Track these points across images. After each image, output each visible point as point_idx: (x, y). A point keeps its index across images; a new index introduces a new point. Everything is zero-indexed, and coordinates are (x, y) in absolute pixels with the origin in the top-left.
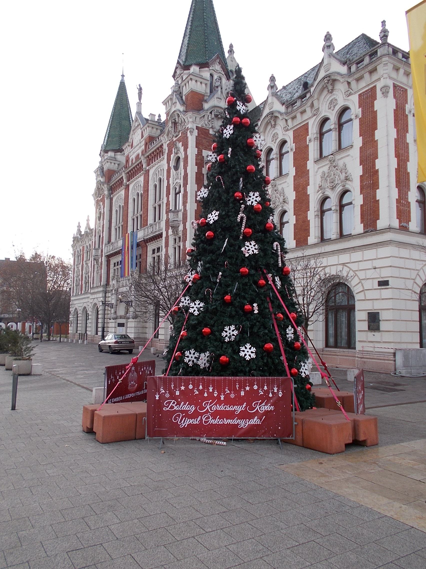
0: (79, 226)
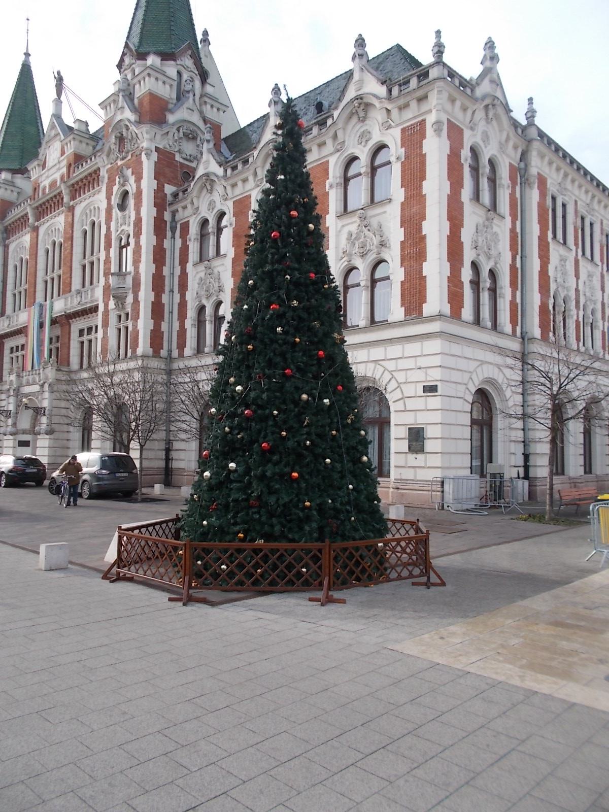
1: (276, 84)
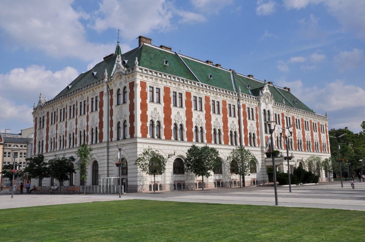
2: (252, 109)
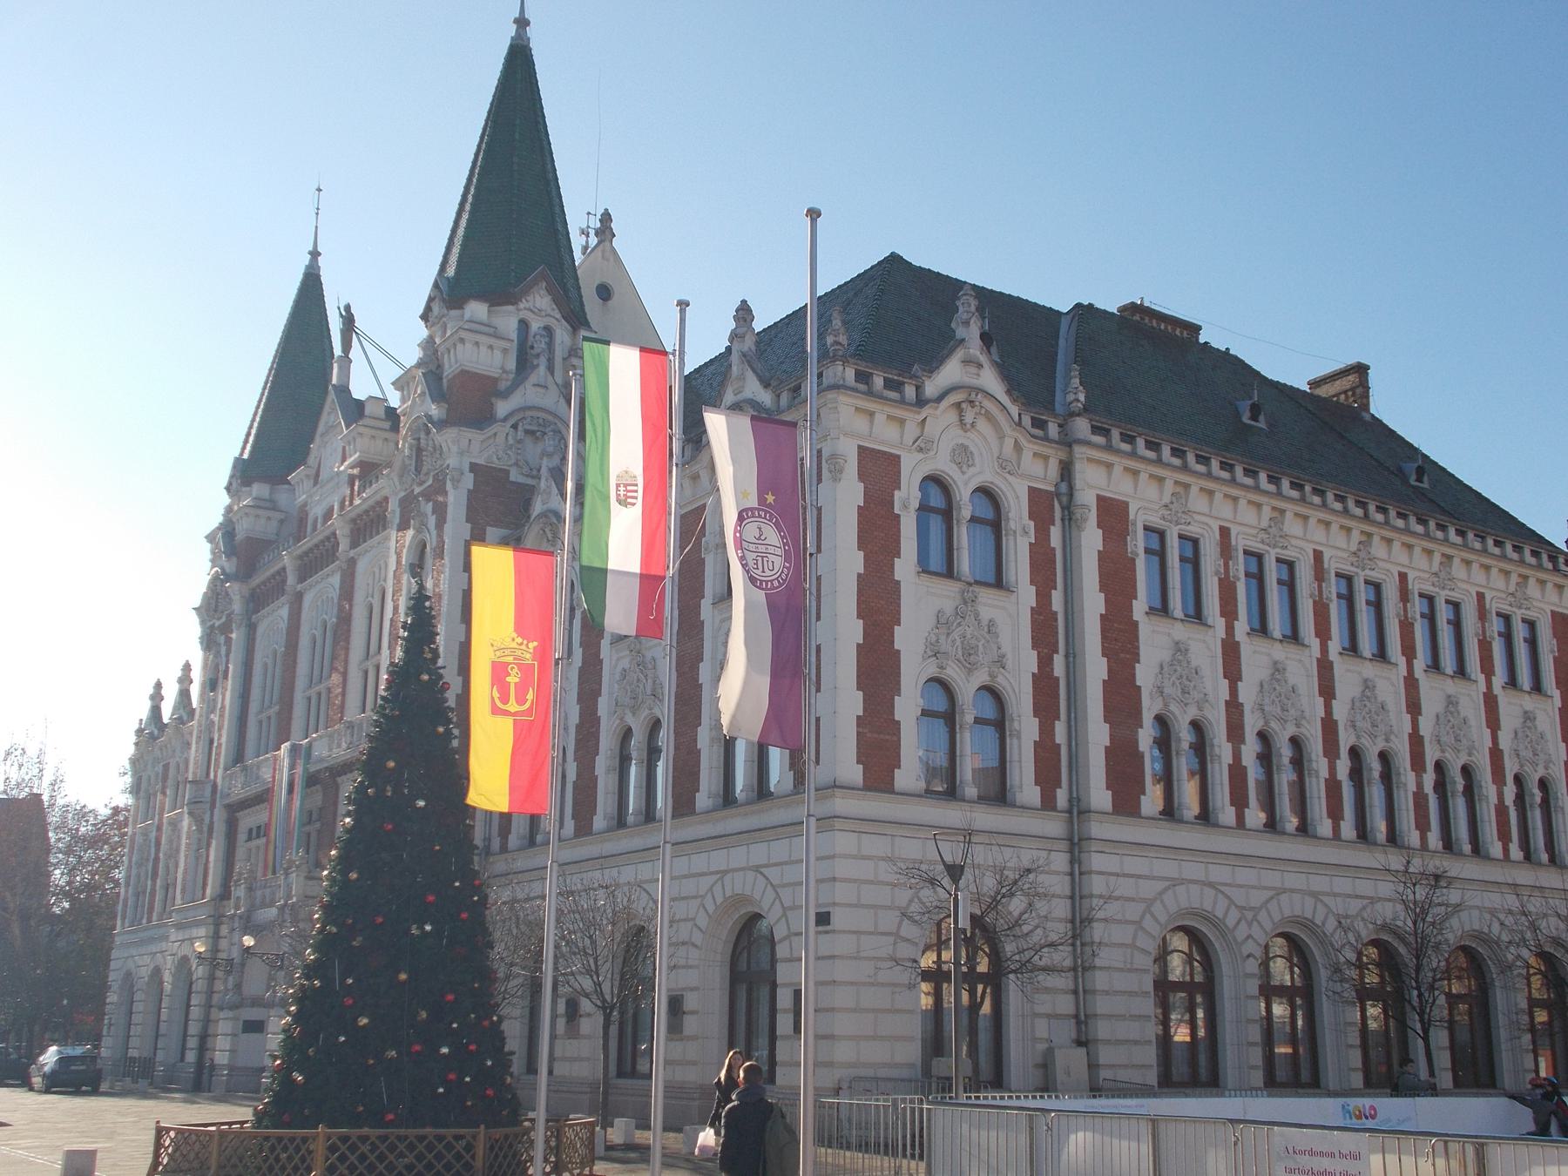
0: (157, 697)
1: (744, 302)
2: (1531, 625)
